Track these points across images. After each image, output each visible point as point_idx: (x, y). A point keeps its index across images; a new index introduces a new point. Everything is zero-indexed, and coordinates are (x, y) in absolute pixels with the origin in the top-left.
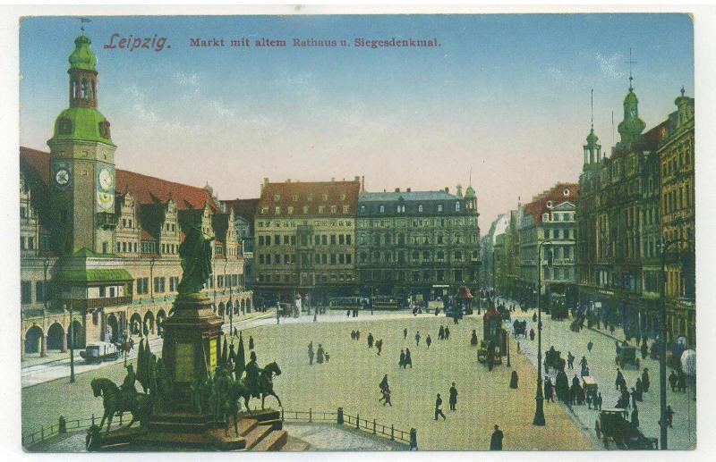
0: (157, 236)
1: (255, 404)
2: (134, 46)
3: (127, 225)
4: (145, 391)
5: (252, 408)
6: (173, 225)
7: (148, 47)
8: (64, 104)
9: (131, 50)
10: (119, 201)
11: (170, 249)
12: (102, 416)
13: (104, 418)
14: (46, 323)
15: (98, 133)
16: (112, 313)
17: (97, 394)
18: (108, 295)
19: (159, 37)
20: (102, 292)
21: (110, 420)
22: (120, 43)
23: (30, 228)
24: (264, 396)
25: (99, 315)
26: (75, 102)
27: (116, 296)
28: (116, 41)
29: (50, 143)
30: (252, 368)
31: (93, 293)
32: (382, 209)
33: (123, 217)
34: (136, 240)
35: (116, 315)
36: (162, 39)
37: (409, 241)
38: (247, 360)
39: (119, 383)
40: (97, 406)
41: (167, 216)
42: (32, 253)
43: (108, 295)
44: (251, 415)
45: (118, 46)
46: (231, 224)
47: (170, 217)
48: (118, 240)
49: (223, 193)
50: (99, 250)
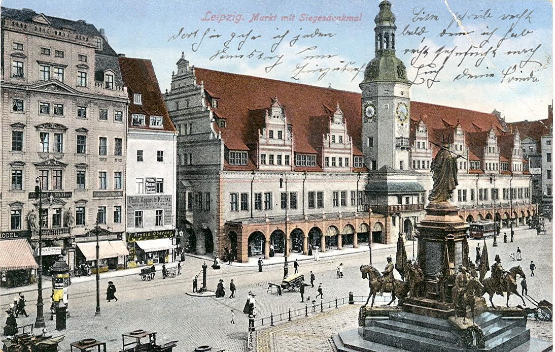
0: (482, 157)
1: (499, 301)
2: (221, 20)
3: (421, 146)
4: (402, 278)
5: (496, 305)
6: (493, 148)
7: (230, 21)
8: (372, 56)
9: (219, 22)
10: (414, 126)
11: (495, 167)
12: (368, 295)
13: (370, 296)
14: (357, 223)
15: (396, 75)
16: (408, 218)
17: (364, 276)
18: (404, 203)
19: (238, 13)
20: (399, 201)
21: (374, 297)
22: (212, 17)
23: (287, 148)
24: (509, 295)
25: (397, 218)
26: (380, 53)
27: (410, 203)
28: (210, 16)
29: (361, 86)
30: (497, 271)
31: (392, 201)
32: (412, 129)
33: (417, 140)
34: (498, 162)
35: (411, 219)
36: (239, 15)
37: (326, 152)
38: (492, 262)
39: (381, 270)
40: (363, 287)
41: (456, 138)
42: (466, 171)
43: (404, 203)
44: (495, 310)
45: (210, 20)
46: (517, 145)
47: (492, 142)
48: (413, 158)
49: (512, 115)
50: (397, 167)
